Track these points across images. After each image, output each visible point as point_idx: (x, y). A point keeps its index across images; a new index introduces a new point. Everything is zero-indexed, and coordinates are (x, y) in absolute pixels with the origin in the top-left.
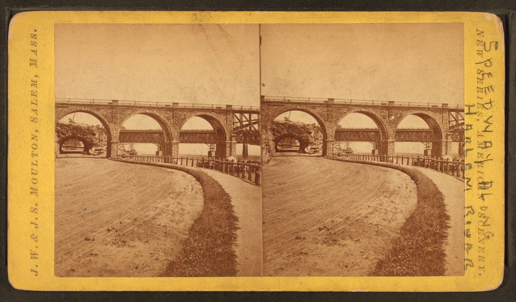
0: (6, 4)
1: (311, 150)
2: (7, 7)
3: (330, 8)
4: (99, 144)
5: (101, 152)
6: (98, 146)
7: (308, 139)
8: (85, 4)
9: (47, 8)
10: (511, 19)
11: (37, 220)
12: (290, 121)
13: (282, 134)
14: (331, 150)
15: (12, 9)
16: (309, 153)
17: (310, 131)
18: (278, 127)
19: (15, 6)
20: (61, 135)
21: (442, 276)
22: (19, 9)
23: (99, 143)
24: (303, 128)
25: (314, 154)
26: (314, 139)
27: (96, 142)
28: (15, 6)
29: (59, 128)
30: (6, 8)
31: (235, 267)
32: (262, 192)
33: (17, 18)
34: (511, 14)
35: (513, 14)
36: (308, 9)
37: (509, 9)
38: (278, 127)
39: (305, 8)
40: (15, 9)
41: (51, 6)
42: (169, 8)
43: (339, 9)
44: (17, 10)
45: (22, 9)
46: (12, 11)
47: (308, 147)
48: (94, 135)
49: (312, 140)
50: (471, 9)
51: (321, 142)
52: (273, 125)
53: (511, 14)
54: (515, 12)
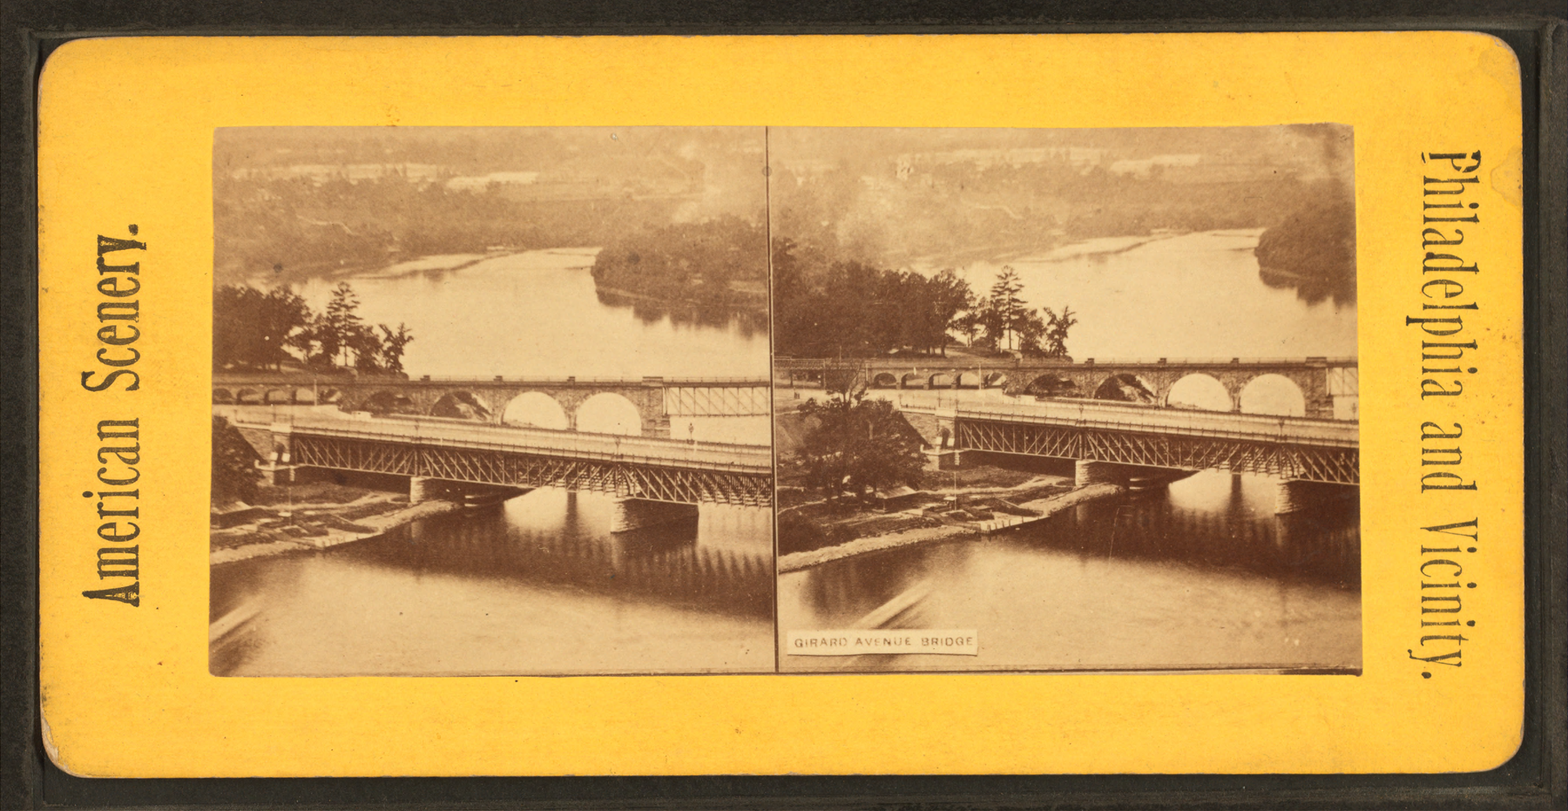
0: (23, 19)
2: (27, 30)
3: (1004, 18)
8: (261, 18)
9: (239, 30)
10: (1550, 43)
11: (1501, 339)
15: (44, 36)
19: (50, 27)
21: (215, 213)
22: (64, 36)
28: (50, 27)
30: (25, 31)
31: (903, 280)
32: (1287, 278)
33: (59, 54)
34: (1550, 30)
35: (1558, 29)
36: (938, 21)
39: (927, 20)
40: (51, 36)
41: (159, 25)
42: (517, 26)
43: (1031, 20)
44: (57, 37)
45: (72, 35)
46: (41, 42)
50: (419, 30)
53: (1550, 30)
54: (1563, 22)
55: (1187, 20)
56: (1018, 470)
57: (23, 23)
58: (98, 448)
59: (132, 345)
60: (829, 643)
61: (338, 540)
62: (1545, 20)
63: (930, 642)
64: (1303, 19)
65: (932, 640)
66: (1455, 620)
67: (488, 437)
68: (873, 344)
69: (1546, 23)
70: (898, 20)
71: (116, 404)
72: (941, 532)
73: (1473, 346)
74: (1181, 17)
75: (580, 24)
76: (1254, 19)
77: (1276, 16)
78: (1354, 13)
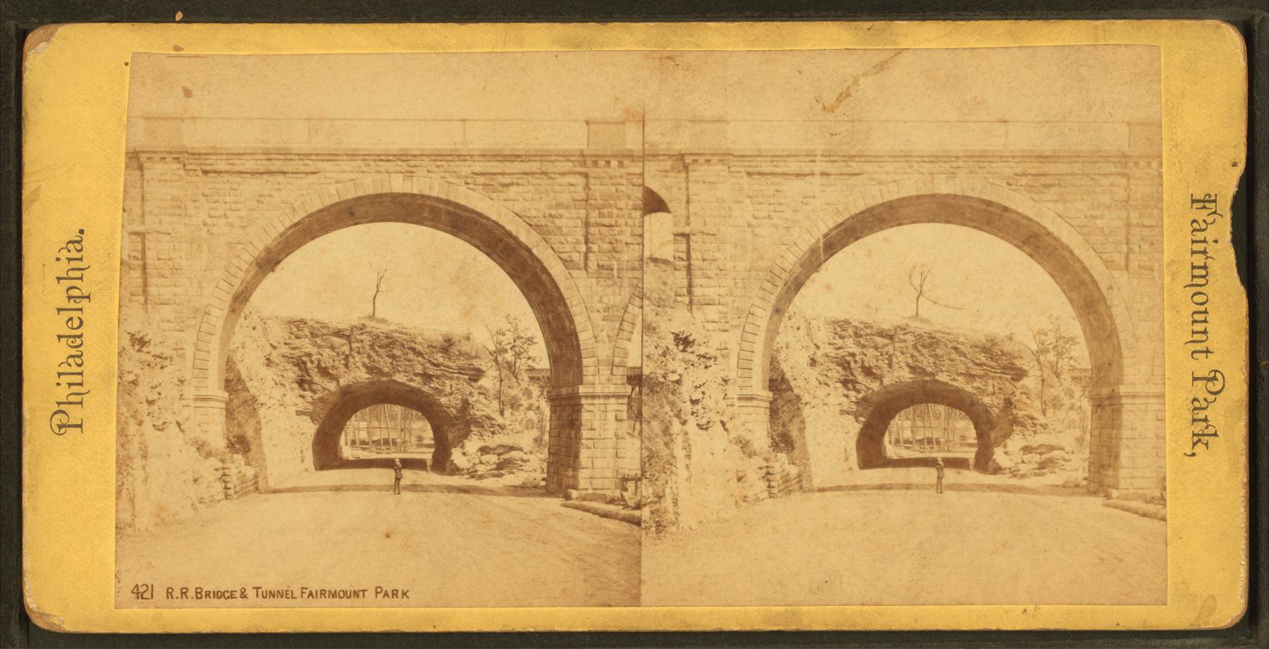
0: (11, 14)
2: (14, 22)
4: (500, 420)
5: (1051, 461)
6: (1038, 427)
7: (466, 405)
12: (383, 321)
13: (886, 381)
14: (610, 452)
16: (1014, 473)
17: (1018, 363)
18: (320, 347)
19: (33, 19)
20: (860, 378)
23: (1044, 412)
24: (985, 350)
25: (501, 475)
26: (495, 404)
27: (488, 411)
28: (33, 19)
29: (850, 346)
36: (757, 14)
37: (1252, 7)
38: (864, 347)
39: (748, 13)
43: (833, 13)
47: (1009, 442)
48: (1019, 374)
49: (484, 407)
52: (298, 337)
54: (1266, 15)
55: (961, 12)
56: (553, 411)
59: (80, 349)
61: (427, 497)
62: (1252, 12)
64: (1054, 12)
66: (72, 262)
67: (453, 484)
68: (991, 319)
69: (1253, 16)
71: (1203, 366)
74: (955, 11)
75: (465, 17)
76: (1014, 12)
77: (1033, 9)
78: (1097, 7)
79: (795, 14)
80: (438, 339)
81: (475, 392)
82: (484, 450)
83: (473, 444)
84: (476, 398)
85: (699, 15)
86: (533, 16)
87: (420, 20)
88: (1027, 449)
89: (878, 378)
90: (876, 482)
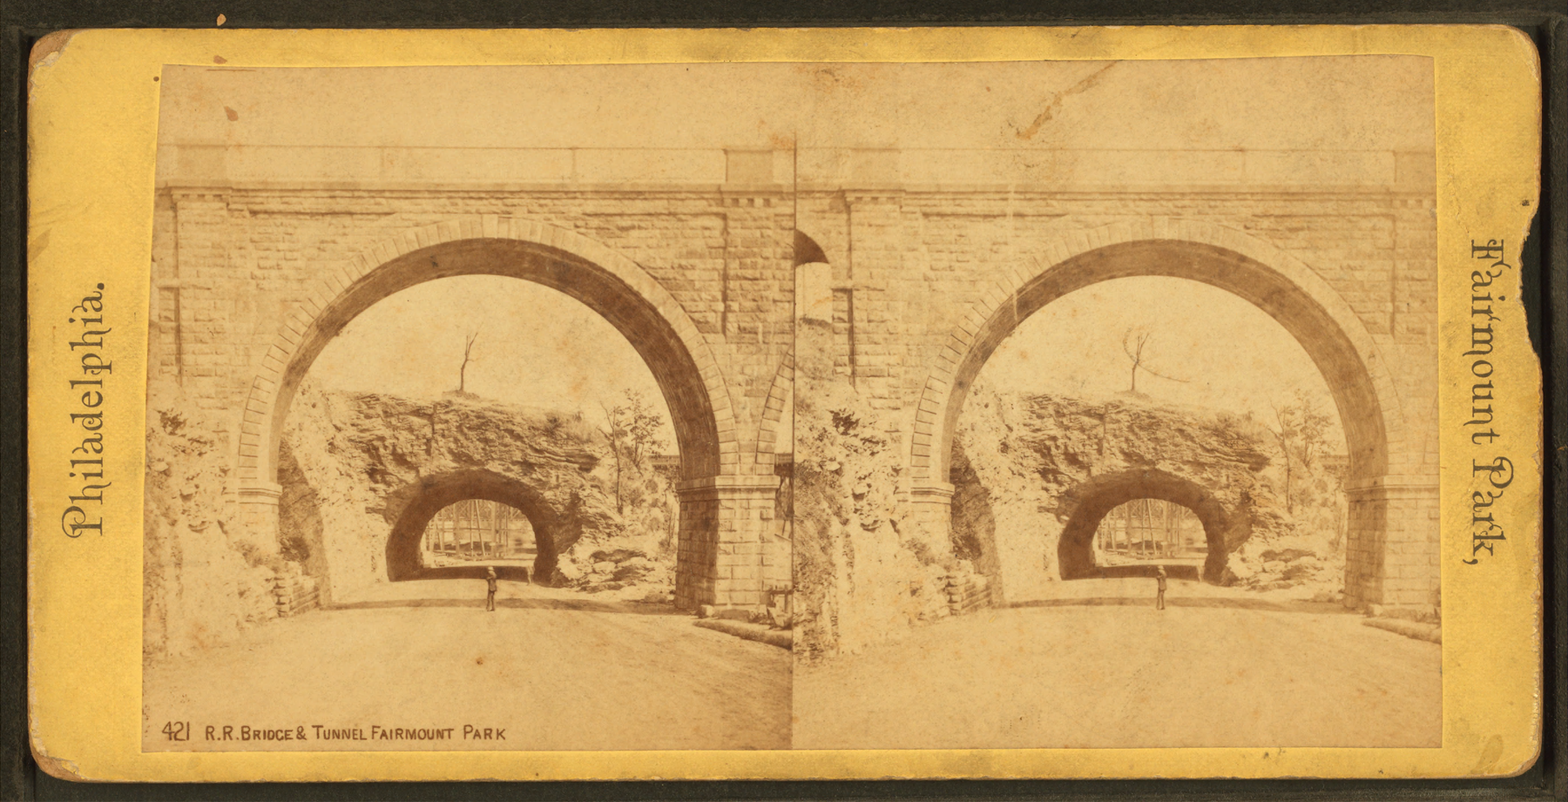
0: (13, 17)
1: (1268, 566)
4: (618, 519)
7: (575, 500)
8: (253, 15)
12: (474, 397)
13: (1095, 471)
14: (754, 558)
16: (1253, 584)
17: (1258, 448)
18: (395, 428)
19: (41, 24)
20: (1063, 467)
23: (1290, 510)
24: (1217, 432)
25: (619, 588)
26: (612, 500)
27: (603, 509)
28: (41, 24)
29: (1051, 427)
36: (936, 17)
37: (1547, 9)
38: (1067, 428)
39: (924, 16)
43: (1029, 16)
47: (1247, 546)
48: (1259, 462)
49: (597, 504)
51: (1326, 520)
52: (368, 417)
54: (1565, 18)
55: (1187, 15)
56: (684, 508)
57: (13, 21)
58: (1494, 506)
60: (482, 734)
63: (261, 735)
64: (1303, 15)
65: (265, 732)
69: (1548, 20)
70: (896, 16)
71: (1487, 453)
72: (512, 590)
73: (73, 345)
74: (1180, 13)
76: (1253, 15)
77: (1276, 11)
79: (982, 18)
80: (541, 419)
81: (587, 485)
82: (598, 556)
83: (584, 549)
84: (588, 491)
85: (864, 19)
86: (659, 20)
87: (518, 25)
88: (1269, 555)
89: (1085, 467)
90: (1083, 595)
